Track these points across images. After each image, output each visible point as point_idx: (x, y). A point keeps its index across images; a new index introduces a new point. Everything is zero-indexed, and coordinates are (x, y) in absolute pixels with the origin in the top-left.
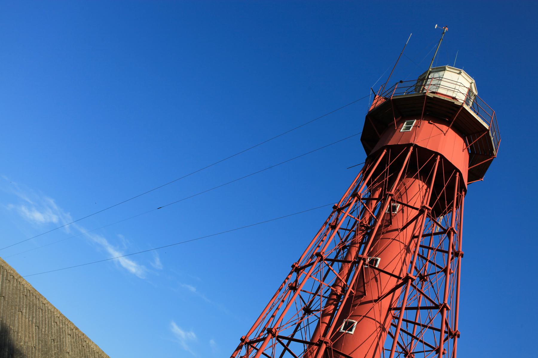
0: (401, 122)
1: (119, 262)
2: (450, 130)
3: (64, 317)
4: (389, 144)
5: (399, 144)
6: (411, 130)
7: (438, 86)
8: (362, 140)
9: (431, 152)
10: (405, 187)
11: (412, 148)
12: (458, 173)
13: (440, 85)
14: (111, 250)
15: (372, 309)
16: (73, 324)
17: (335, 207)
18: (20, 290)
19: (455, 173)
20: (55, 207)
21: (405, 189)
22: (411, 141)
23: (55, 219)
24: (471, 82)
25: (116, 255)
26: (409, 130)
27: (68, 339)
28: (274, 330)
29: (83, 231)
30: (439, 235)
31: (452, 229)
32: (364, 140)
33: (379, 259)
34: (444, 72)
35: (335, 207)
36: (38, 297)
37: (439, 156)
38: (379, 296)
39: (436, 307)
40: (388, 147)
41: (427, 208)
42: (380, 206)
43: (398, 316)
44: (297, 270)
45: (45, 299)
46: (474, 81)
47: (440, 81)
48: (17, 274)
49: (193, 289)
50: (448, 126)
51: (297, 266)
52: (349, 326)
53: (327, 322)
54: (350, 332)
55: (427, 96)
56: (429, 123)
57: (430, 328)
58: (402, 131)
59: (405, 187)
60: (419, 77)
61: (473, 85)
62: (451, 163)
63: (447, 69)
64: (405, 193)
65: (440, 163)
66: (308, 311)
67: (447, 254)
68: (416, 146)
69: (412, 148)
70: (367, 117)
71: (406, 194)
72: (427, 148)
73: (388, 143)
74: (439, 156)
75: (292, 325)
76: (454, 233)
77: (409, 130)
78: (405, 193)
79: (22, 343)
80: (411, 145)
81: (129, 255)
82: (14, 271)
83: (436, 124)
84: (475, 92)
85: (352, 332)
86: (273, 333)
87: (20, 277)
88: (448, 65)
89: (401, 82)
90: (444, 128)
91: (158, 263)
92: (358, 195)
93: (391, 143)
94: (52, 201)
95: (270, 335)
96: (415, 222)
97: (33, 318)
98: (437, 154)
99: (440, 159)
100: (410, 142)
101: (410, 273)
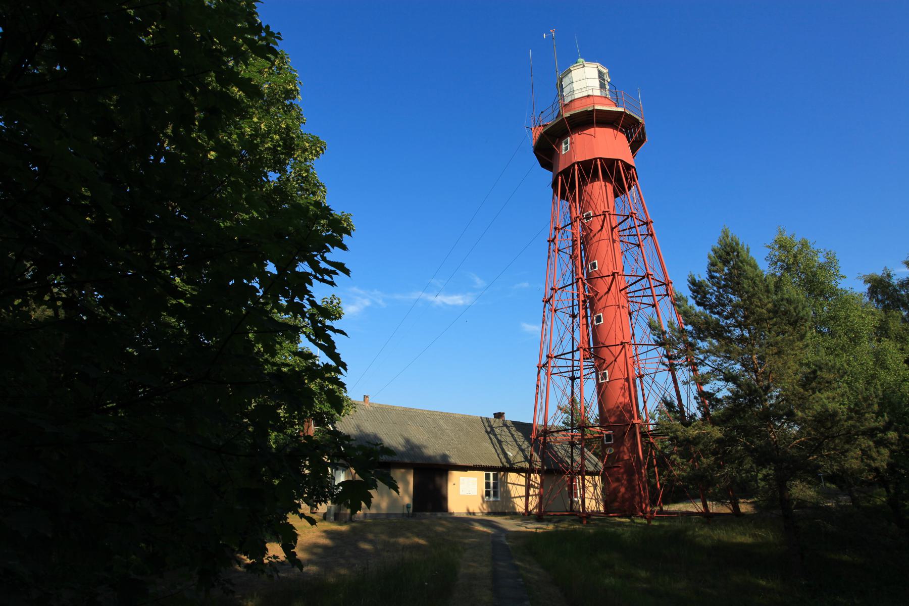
0: (559, 145)
1: (444, 303)
2: (597, 129)
3: (430, 411)
4: (559, 171)
8: (542, 166)
9: (591, 161)
10: (588, 193)
11: (576, 167)
14: (431, 298)
16: (438, 412)
17: (549, 241)
18: (399, 414)
19: (617, 163)
20: (361, 292)
21: (588, 196)
22: (573, 161)
23: (367, 303)
24: (596, 66)
25: (441, 299)
27: (441, 422)
28: (550, 355)
29: (398, 297)
32: (543, 166)
33: (596, 261)
34: (571, 73)
36: (410, 410)
38: (539, 364)
41: (606, 212)
44: (547, 301)
45: (414, 409)
46: (598, 64)
48: (391, 406)
49: (526, 285)
50: (593, 127)
51: (545, 300)
52: (599, 319)
53: (585, 323)
54: (601, 323)
55: (566, 117)
56: (579, 134)
57: (640, 296)
58: (563, 153)
59: (588, 193)
61: (600, 67)
63: (572, 69)
65: (602, 165)
66: (573, 316)
68: (578, 163)
69: (576, 167)
70: (534, 152)
72: (587, 159)
73: (558, 169)
74: (598, 160)
79: (422, 440)
80: (574, 163)
81: (450, 291)
82: (388, 406)
83: (585, 132)
85: (602, 322)
87: (394, 407)
88: (572, 65)
89: (542, 112)
90: (591, 131)
91: (479, 282)
93: (560, 169)
94: (355, 289)
95: (550, 359)
97: (416, 424)
98: (596, 159)
99: (600, 161)
100: (573, 162)
101: (614, 269)
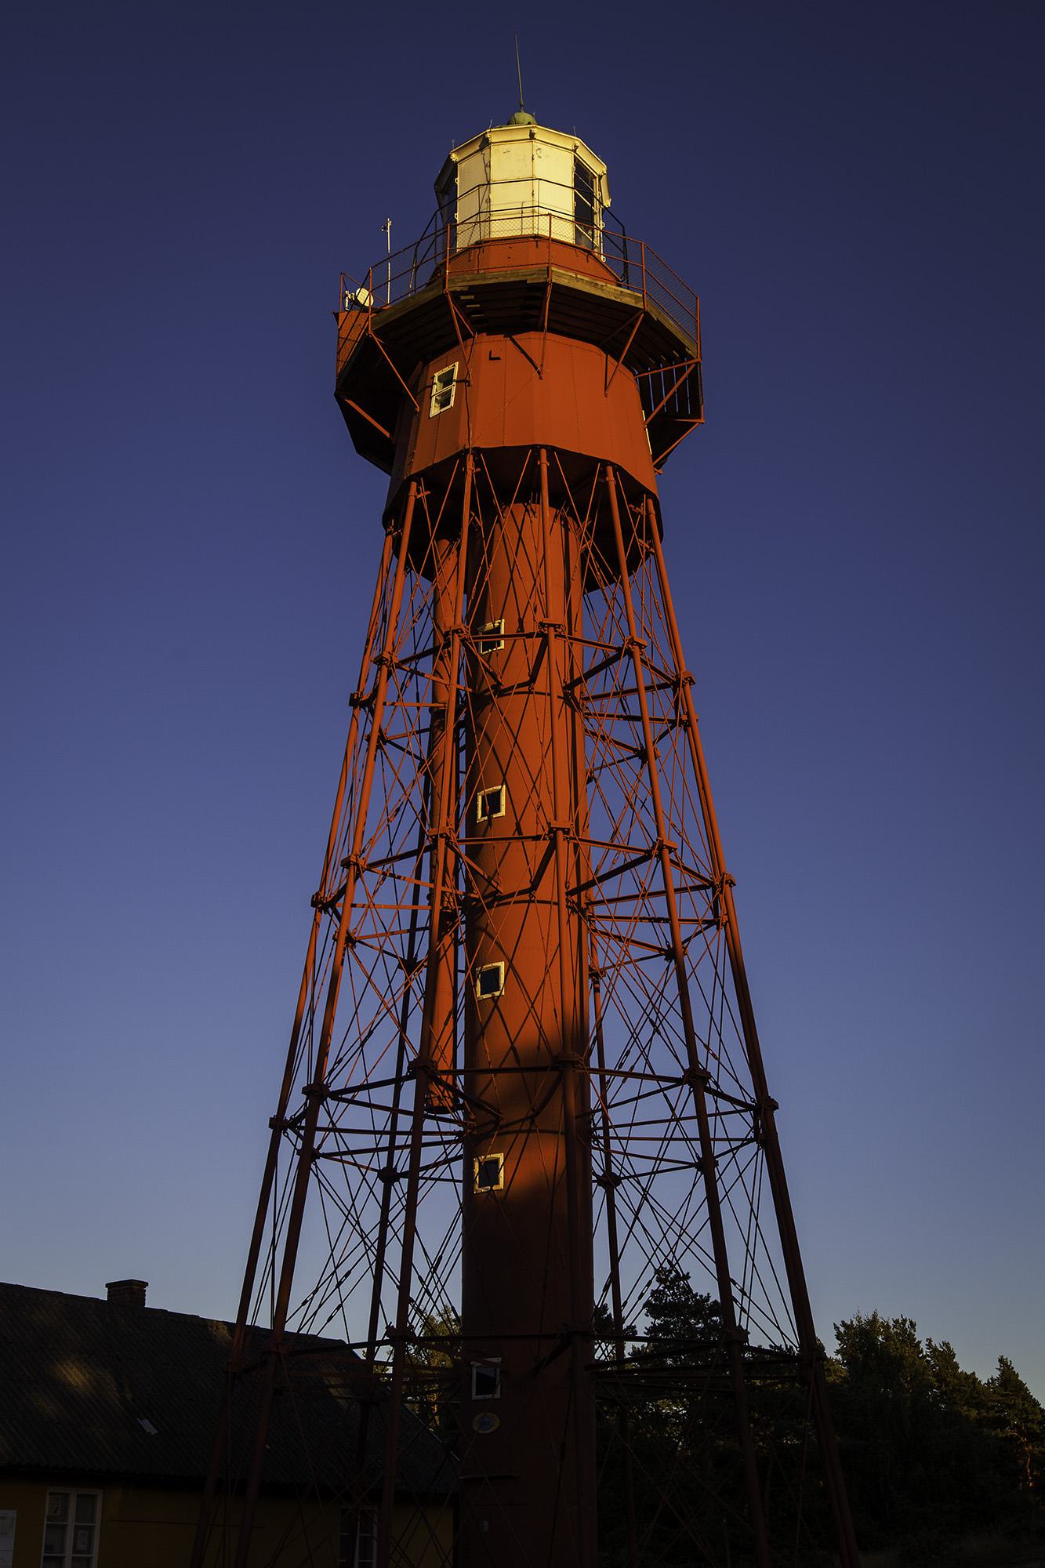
5: (435, 462)
6: (452, 403)
7: (484, 215)
9: (523, 449)
12: (610, 469)
13: (490, 211)
15: (494, 1013)
19: (604, 474)
22: (463, 443)
24: (571, 147)
26: (449, 407)
30: (632, 861)
31: (632, 642)
35: (355, 702)
37: (544, 452)
39: (647, 856)
40: (416, 477)
42: (432, 1052)
43: (557, 901)
46: (578, 142)
47: (487, 223)
60: (435, 185)
62: (581, 454)
63: (493, 138)
64: (496, 1010)
65: (552, 470)
67: (641, 723)
68: (477, 451)
71: (498, 1013)
74: (544, 452)
75: (375, 760)
76: (640, 648)
77: (449, 407)
78: (496, 1010)
84: (598, 167)
86: (316, 1094)
92: (387, 660)
96: (521, 542)
98: (536, 449)
99: (550, 458)
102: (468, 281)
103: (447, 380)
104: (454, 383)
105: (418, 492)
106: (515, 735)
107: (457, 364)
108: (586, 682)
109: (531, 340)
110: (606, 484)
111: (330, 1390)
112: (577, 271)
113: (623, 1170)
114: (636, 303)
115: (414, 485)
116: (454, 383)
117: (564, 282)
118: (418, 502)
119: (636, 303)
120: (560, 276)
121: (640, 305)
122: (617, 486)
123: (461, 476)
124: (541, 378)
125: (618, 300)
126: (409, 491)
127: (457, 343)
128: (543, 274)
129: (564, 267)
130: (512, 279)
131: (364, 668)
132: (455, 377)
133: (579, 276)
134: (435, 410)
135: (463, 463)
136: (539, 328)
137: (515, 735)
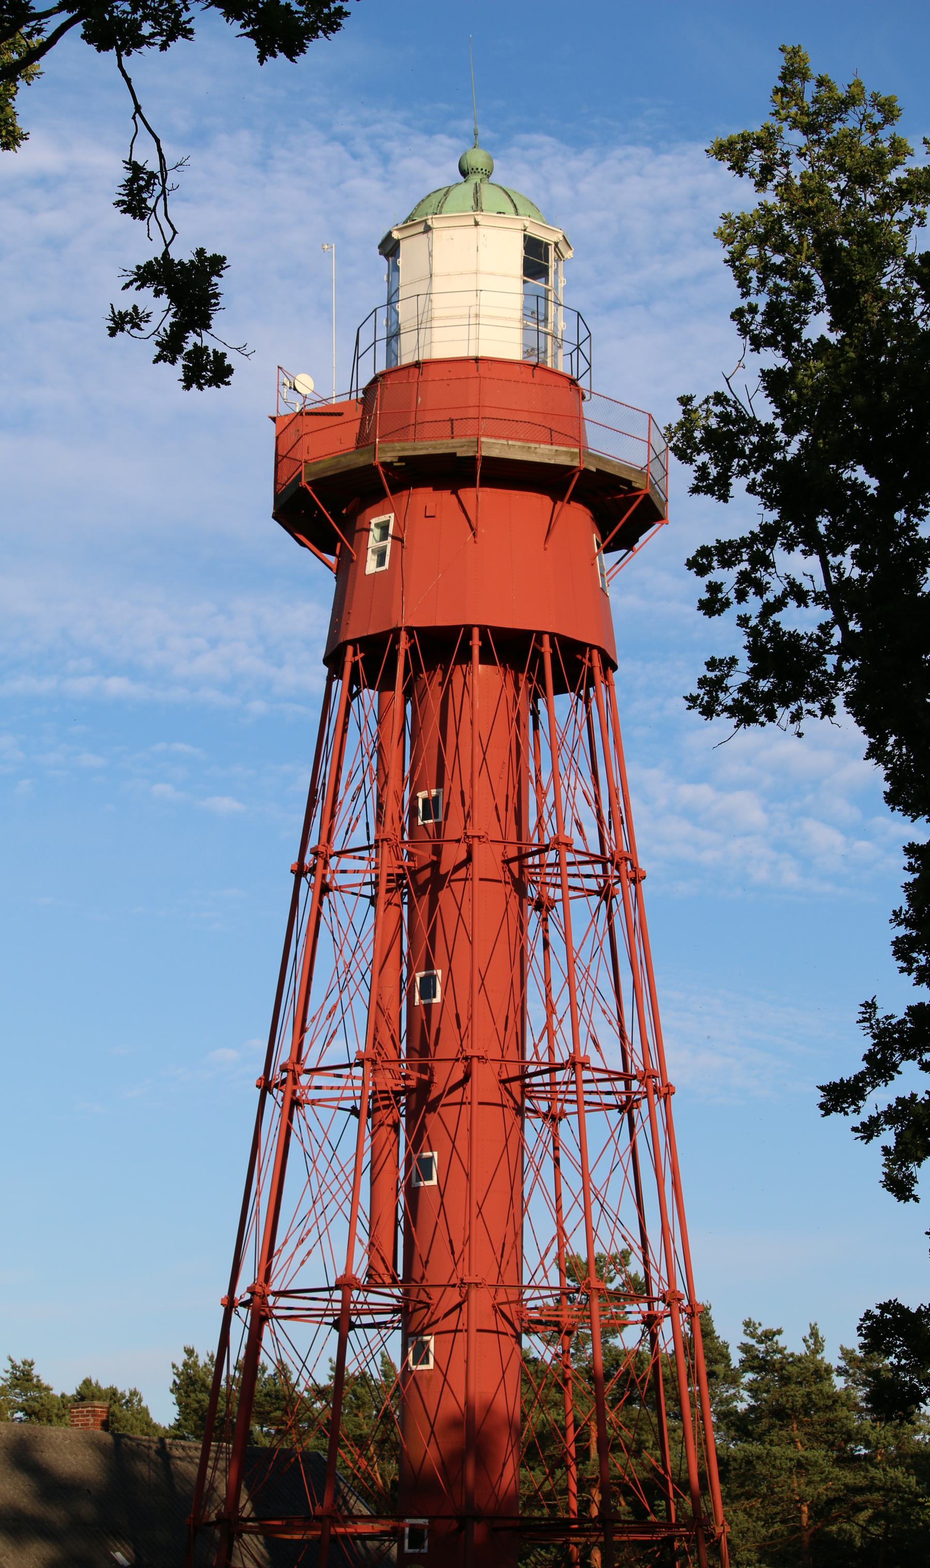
68: (410, 630)
102: (399, 451)
103: (384, 527)
104: (390, 539)
105: (355, 654)
106: (444, 1371)
107: (392, 515)
108: (568, 502)
109: (467, 494)
110: (541, 655)
111: (369, 1513)
112: (508, 438)
113: (618, 1223)
114: (572, 460)
115: (350, 649)
116: (390, 539)
117: (495, 453)
118: (355, 665)
119: (572, 460)
120: (491, 446)
121: (576, 463)
122: (554, 656)
123: (394, 654)
124: (475, 542)
125: (552, 462)
126: (345, 655)
127: (386, 496)
128: (472, 447)
129: (491, 436)
130: (441, 451)
131: (418, 1396)
132: (391, 531)
133: (510, 442)
134: (371, 566)
135: (397, 640)
136: (473, 485)
137: (444, 1371)
